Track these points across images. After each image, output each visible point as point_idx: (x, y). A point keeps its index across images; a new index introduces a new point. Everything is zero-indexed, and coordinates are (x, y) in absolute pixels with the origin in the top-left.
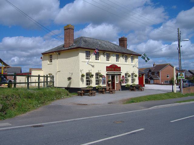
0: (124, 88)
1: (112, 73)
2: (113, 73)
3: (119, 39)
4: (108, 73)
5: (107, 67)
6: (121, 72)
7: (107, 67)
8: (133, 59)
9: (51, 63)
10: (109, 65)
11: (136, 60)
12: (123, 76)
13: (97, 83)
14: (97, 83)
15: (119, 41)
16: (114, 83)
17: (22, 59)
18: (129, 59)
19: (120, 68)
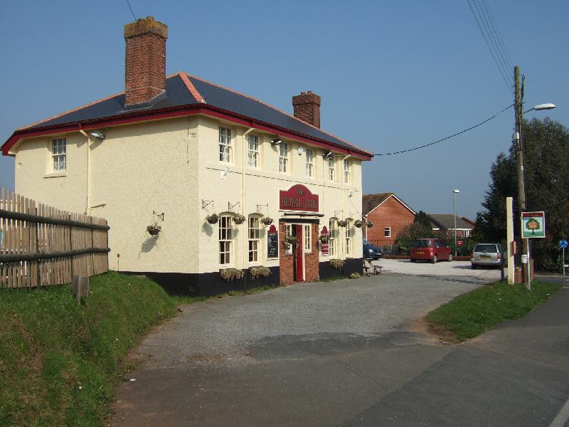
0: (330, 271)
1: (294, 214)
2: (299, 217)
3: (294, 98)
4: (285, 215)
5: (282, 193)
6: (320, 212)
7: (282, 193)
8: (348, 162)
9: (62, 172)
10: (287, 189)
11: (356, 169)
12: (325, 228)
13: (224, 231)
14: (224, 231)
15: (294, 105)
16: (300, 250)
17: (480, 286)
18: (340, 164)
19: (316, 197)
